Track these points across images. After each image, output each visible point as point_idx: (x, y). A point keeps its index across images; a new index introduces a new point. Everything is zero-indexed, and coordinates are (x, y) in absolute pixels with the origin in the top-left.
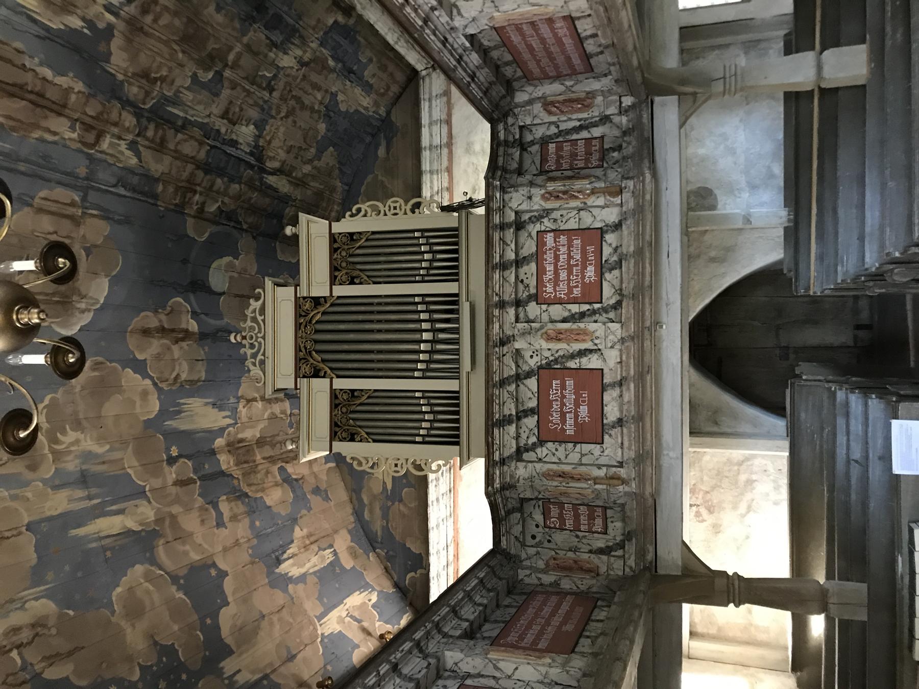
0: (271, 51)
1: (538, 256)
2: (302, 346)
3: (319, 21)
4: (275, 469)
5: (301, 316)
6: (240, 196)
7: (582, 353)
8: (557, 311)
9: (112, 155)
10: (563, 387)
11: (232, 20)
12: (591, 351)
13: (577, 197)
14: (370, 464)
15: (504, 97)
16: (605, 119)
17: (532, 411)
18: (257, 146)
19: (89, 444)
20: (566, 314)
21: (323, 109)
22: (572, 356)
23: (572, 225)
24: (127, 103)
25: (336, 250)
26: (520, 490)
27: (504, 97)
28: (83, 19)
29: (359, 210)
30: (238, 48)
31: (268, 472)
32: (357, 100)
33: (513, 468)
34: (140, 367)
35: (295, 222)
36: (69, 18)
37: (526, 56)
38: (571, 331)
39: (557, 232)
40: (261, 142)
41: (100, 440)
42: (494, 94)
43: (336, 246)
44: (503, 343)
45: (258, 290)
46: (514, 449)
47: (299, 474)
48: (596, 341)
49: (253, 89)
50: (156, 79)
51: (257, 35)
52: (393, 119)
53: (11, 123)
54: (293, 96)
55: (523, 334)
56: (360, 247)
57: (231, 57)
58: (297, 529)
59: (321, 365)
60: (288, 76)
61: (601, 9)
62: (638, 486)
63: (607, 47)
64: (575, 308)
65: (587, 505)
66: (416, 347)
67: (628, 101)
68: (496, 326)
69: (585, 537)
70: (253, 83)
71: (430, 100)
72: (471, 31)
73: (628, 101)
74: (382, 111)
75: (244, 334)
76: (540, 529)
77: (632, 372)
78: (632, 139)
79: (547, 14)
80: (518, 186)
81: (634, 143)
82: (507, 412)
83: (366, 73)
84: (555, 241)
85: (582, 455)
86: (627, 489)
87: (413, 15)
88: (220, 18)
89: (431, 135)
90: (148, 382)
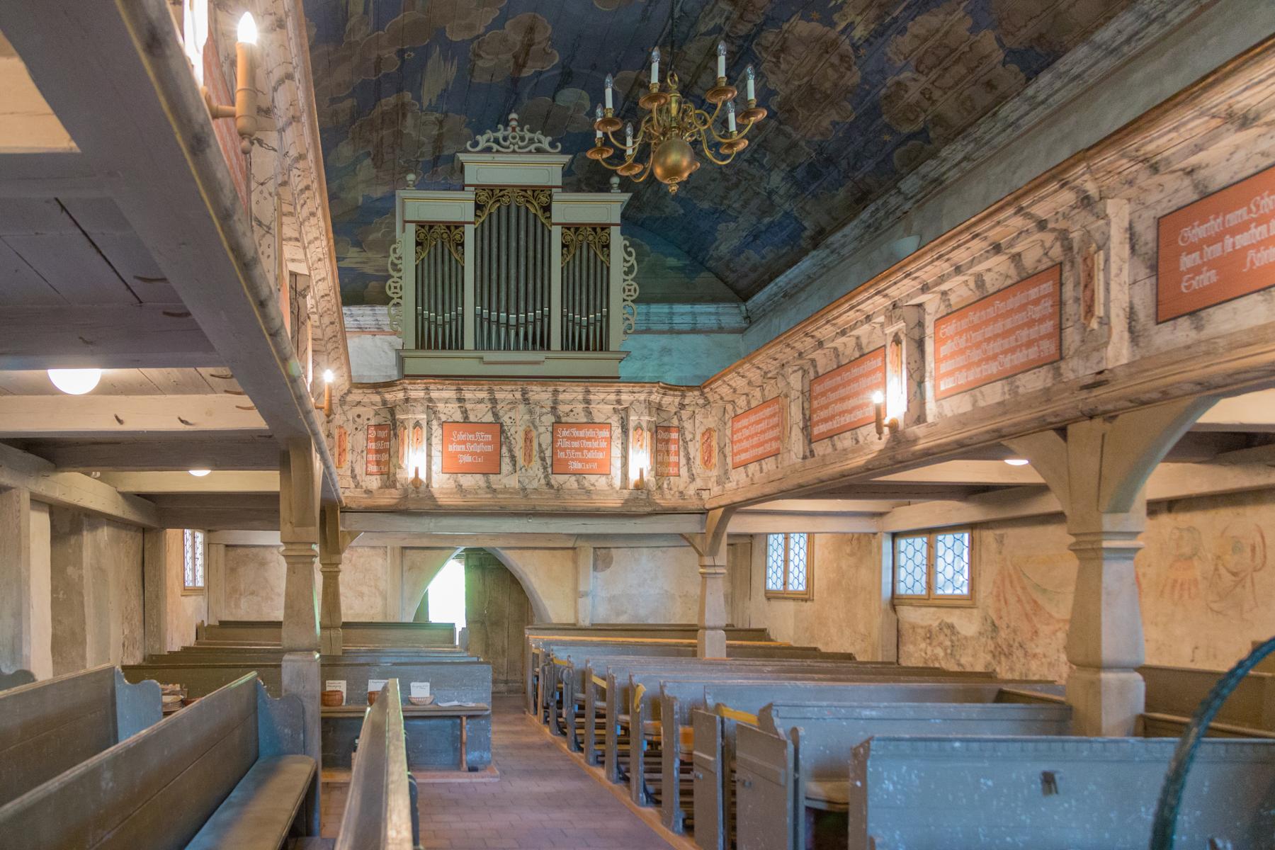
7: (513, 458)
8: (546, 439)
9: (711, 11)
11: (822, 134)
12: (514, 465)
20: (544, 446)
22: (510, 451)
24: (760, 28)
25: (594, 229)
29: (630, 254)
30: (796, 136)
32: (727, 240)
34: (498, 23)
43: (598, 230)
45: (559, 145)
50: (778, 58)
52: (702, 274)
54: (740, 181)
57: (788, 129)
59: (487, 212)
62: (413, 499)
64: (548, 453)
66: (503, 309)
71: (717, 314)
74: (712, 264)
75: (518, 129)
88: (826, 123)
89: (683, 314)
90: (482, 30)
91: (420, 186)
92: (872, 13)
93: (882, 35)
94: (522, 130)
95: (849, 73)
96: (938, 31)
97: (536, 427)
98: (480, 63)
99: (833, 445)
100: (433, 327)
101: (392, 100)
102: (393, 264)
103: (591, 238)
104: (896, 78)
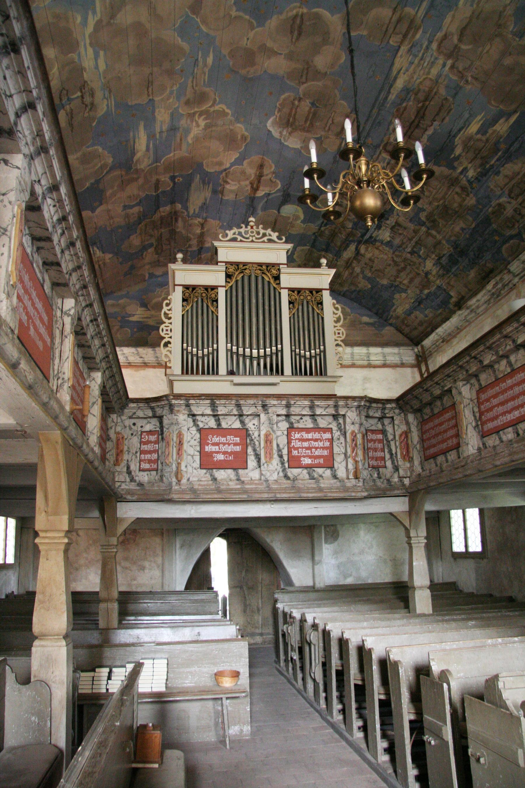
0: (436, 256)
1: (317, 429)
2: (247, 267)
3: (453, 287)
4: (153, 241)
5: (267, 267)
6: (344, 228)
8: (283, 441)
10: (235, 444)
11: (455, 235)
13: (353, 452)
14: (167, 312)
15: (412, 408)
16: (396, 468)
17: (219, 425)
18: (375, 240)
19: (195, 131)
20: (281, 446)
21: (397, 283)
22: (255, 450)
23: (336, 450)
26: (170, 416)
27: (412, 408)
28: (460, 155)
29: (337, 309)
31: (151, 236)
32: (402, 304)
33: (183, 412)
34: (239, 161)
35: (330, 265)
36: (461, 148)
37: (437, 422)
38: (272, 449)
39: (331, 440)
40: (378, 244)
41: (197, 139)
42: (415, 402)
43: (314, 292)
44: (264, 406)
46: (196, 413)
47: (146, 256)
48: (265, 465)
49: (413, 243)
51: (447, 249)
52: (387, 328)
53: (402, 110)
55: (270, 420)
56: (313, 309)
57: (434, 232)
58: (110, 256)
59: (234, 280)
60: (420, 264)
61: (463, 464)
62: (176, 490)
63: (441, 468)
64: (285, 452)
65: (158, 459)
67: (407, 481)
68: (275, 402)
69: (136, 457)
70: (416, 243)
72: (454, 391)
73: (407, 481)
74: (392, 321)
75: (254, 227)
76: (140, 429)
77: (247, 486)
78: (384, 485)
79: (462, 434)
80: (360, 416)
81: (383, 486)
82: (219, 408)
83: (418, 312)
84: (326, 439)
85: (192, 456)
86: (174, 484)
87: (465, 361)
88: (457, 229)
91: (185, 261)
92: (478, 162)
93: (485, 175)
94: (258, 228)
95: (468, 198)
96: (518, 173)
97: (274, 431)
98: (228, 187)
99: (500, 439)
100: (195, 358)
101: (168, 208)
102: (165, 314)
103: (309, 298)
104: (497, 201)
